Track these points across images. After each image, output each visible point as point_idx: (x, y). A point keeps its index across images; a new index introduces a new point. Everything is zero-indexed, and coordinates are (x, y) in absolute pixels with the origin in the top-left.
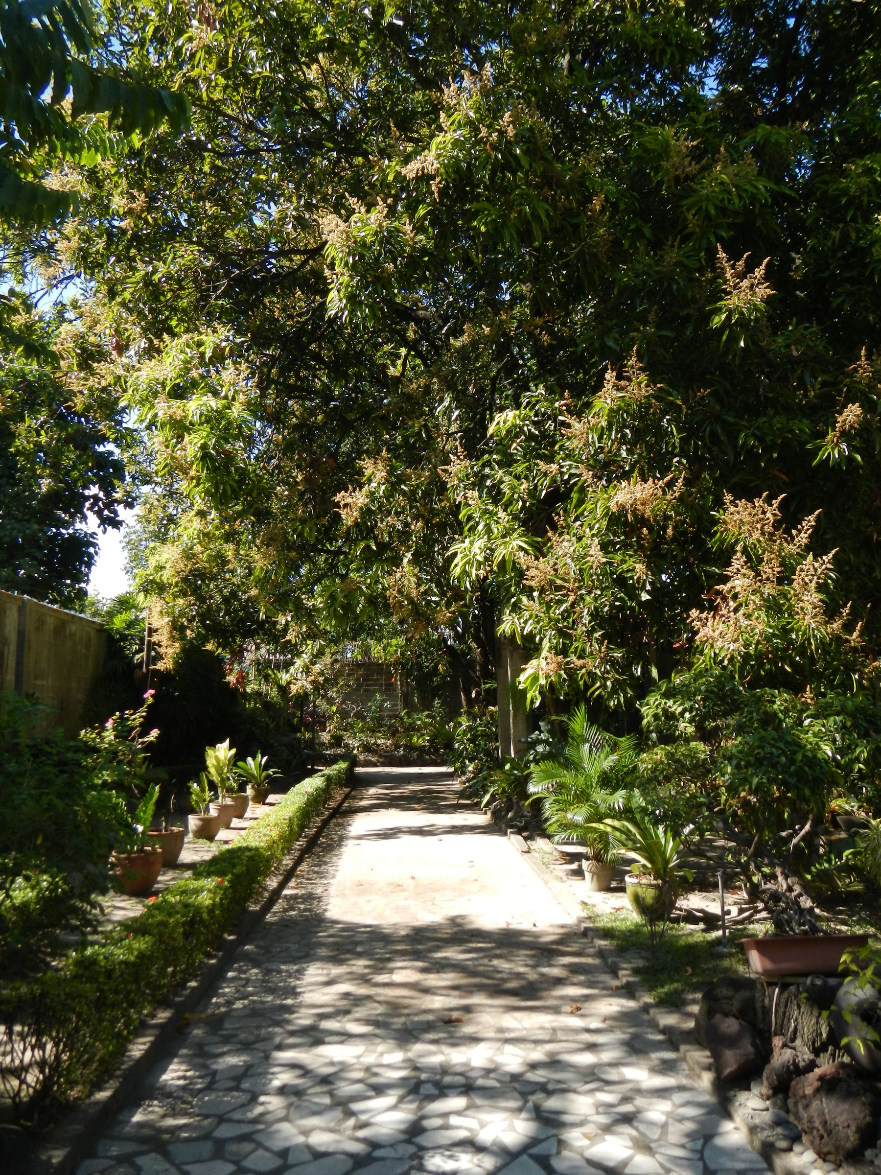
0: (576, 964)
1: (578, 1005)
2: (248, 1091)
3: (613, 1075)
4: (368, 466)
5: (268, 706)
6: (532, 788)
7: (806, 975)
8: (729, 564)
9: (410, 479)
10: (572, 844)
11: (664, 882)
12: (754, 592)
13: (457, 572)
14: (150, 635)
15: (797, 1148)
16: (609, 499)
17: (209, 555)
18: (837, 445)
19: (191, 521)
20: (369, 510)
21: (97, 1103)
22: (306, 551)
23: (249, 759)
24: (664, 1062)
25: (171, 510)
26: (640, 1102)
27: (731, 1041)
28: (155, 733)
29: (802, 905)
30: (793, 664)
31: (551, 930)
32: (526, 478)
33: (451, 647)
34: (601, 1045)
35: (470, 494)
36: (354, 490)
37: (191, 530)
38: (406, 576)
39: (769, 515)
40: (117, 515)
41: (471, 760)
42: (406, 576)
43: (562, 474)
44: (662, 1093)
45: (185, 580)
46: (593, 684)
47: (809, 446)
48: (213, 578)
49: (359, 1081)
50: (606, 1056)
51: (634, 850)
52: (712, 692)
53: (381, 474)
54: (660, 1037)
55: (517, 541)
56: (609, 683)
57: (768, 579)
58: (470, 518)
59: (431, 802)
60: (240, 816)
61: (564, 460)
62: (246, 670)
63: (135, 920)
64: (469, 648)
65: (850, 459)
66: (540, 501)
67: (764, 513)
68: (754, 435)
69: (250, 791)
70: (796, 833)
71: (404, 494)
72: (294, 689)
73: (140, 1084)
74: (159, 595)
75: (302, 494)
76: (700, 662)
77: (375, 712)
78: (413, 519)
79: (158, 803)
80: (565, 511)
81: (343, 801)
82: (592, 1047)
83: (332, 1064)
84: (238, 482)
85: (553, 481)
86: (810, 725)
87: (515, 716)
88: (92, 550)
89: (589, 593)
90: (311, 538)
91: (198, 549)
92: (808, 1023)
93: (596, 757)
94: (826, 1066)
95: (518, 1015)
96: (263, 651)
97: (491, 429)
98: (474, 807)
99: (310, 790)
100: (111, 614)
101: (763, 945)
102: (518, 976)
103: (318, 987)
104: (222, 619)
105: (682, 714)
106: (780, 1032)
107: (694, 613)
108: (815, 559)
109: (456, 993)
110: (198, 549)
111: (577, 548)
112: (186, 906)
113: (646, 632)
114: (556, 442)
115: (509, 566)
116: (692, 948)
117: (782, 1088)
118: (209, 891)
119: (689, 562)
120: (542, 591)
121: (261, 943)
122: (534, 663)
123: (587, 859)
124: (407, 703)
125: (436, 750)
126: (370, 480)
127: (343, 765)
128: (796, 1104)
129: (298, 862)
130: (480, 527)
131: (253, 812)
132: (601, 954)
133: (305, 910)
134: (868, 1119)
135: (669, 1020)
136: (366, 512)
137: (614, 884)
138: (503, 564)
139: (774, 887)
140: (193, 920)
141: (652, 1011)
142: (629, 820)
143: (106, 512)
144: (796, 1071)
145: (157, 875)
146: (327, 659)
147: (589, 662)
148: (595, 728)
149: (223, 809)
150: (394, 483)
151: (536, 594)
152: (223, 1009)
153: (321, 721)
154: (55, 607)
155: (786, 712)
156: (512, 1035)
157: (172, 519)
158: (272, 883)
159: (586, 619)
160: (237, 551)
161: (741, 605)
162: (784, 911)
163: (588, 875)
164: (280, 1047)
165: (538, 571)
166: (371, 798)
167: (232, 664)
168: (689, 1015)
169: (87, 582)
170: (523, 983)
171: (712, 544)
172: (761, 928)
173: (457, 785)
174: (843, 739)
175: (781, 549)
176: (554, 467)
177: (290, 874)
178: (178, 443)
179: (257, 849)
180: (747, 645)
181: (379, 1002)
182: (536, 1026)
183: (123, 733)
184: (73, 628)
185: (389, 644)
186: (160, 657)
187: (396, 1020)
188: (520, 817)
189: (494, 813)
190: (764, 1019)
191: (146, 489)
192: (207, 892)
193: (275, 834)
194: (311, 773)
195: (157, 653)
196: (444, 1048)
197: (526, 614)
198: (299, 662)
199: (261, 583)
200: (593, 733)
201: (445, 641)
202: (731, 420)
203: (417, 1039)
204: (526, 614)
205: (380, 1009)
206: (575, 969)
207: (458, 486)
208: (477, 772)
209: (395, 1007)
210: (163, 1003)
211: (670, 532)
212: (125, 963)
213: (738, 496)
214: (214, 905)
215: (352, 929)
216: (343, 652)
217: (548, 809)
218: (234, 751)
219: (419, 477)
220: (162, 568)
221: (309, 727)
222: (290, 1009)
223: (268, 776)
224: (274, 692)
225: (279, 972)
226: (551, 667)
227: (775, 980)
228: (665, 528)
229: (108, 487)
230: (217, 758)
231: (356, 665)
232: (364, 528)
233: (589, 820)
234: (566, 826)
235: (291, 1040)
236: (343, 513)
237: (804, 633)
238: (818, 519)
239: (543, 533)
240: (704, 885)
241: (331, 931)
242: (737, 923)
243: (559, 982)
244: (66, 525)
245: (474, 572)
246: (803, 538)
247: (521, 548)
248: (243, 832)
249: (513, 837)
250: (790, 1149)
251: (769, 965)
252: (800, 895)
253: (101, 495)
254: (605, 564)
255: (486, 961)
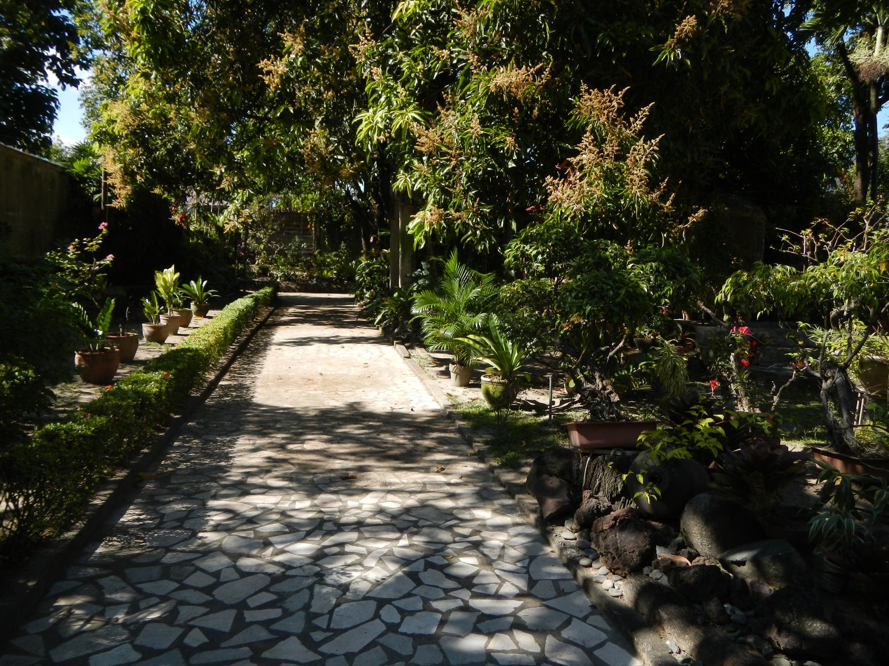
0: (442, 438)
1: (442, 467)
2: (189, 529)
3: (466, 515)
4: (288, 40)
5: (208, 242)
6: (414, 311)
7: (611, 449)
8: (580, 141)
9: (324, 54)
10: (443, 352)
11: (510, 382)
12: (597, 165)
13: (361, 136)
14: (106, 179)
15: (595, 565)
16: (489, 81)
17: (154, 113)
18: (673, 50)
19: (137, 82)
20: (288, 78)
21: (66, 540)
22: (237, 115)
23: (192, 282)
24: (504, 506)
25: (120, 71)
26: (485, 534)
27: (553, 493)
28: (110, 258)
29: (612, 399)
30: (619, 223)
31: (424, 413)
32: (422, 60)
33: (355, 202)
34: (459, 495)
35: (375, 70)
36: (276, 59)
37: (137, 90)
38: (318, 137)
39: (614, 103)
40: (74, 74)
41: (368, 290)
42: (318, 137)
43: (452, 59)
44: (502, 528)
45: (133, 133)
46: (467, 232)
47: (651, 49)
48: (158, 132)
49: (277, 521)
50: (461, 503)
51: (489, 357)
52: (560, 240)
53: (299, 47)
54: (501, 489)
55: (412, 113)
56: (478, 232)
57: (608, 155)
58: (374, 91)
59: (337, 320)
60: (186, 326)
61: (454, 47)
62: (189, 208)
63: (94, 402)
64: (370, 204)
65: (682, 63)
66: (432, 81)
67: (611, 101)
68: (609, 37)
69: (193, 307)
70: (612, 348)
71: (317, 65)
72: (227, 228)
73: (103, 524)
74: (113, 145)
75: (232, 63)
76: (550, 219)
77: (294, 250)
78: (325, 89)
79: (114, 313)
80: (452, 90)
81: (268, 317)
82: (452, 496)
83: (256, 508)
84: (175, 46)
85: (444, 65)
86: (632, 268)
87: (403, 257)
88: (53, 104)
89: (468, 159)
90: (239, 99)
91: (144, 107)
92: (609, 481)
93: (464, 286)
94: (619, 510)
95: (398, 473)
96: (202, 196)
97: (395, 16)
98: (369, 324)
99: (241, 307)
100: (72, 160)
101: (581, 427)
102: (400, 445)
103: (247, 453)
104: (167, 170)
105: (536, 256)
106: (588, 487)
107: (549, 179)
108: (645, 142)
109: (352, 458)
110: (144, 107)
111: (460, 122)
112: (136, 392)
113: (511, 193)
114: (448, 31)
115: (405, 134)
116: (526, 428)
117: (587, 525)
118: (156, 381)
119: (547, 137)
120: (430, 156)
121: (202, 420)
122: (421, 213)
123: (453, 363)
124: (320, 244)
125: (342, 282)
126: (290, 53)
127: (268, 290)
128: (597, 537)
129: (232, 361)
130: (382, 99)
131: (196, 323)
132: (460, 430)
133: (237, 396)
134: (648, 547)
135: (509, 477)
136: (286, 80)
137: (472, 382)
138: (399, 131)
139: (593, 387)
140: (143, 401)
141: (496, 471)
142: (486, 336)
143: (64, 72)
144: (598, 513)
145: (117, 368)
146: (255, 206)
147: (463, 214)
148: (464, 266)
149: (170, 320)
150: (310, 56)
151: (425, 158)
152: (170, 469)
153: (252, 256)
154: (21, 150)
155: (615, 258)
156: (393, 488)
157: (121, 81)
158: (211, 376)
159: (464, 180)
160: (178, 110)
161: (585, 175)
162: (599, 403)
163: (453, 375)
164: (215, 497)
165: (428, 138)
166: (290, 315)
167: (177, 206)
168: (524, 473)
169: (52, 131)
170: (403, 451)
171: (568, 125)
172: (579, 415)
173: (357, 307)
174: (656, 280)
175: (620, 133)
176: (446, 52)
177: (225, 370)
178: (120, 6)
179: (197, 350)
180: (587, 207)
181: (292, 464)
182: (411, 481)
183: (85, 257)
184: (39, 169)
185: (306, 198)
186: (115, 197)
187: (306, 477)
188: (404, 332)
189: (384, 329)
190: (578, 478)
191: (98, 53)
192: (154, 383)
193: (212, 339)
194: (242, 295)
195: (113, 194)
196: (342, 497)
197: (417, 174)
198: (231, 207)
199: (199, 137)
200: (464, 272)
201: (351, 197)
202: (592, 21)
203: (321, 491)
204: (417, 174)
205: (293, 469)
206: (442, 441)
207: (365, 63)
208: (372, 298)
209: (305, 468)
210: (122, 466)
211: (536, 112)
212: (84, 436)
213: (591, 86)
214: (160, 392)
215: (273, 410)
216: (270, 201)
217: (426, 326)
218: (178, 274)
219: (331, 52)
220: (114, 122)
221: (242, 260)
222: (223, 470)
223: (208, 296)
224: (213, 231)
225: (216, 442)
226: (434, 217)
227: (588, 452)
228: (532, 109)
229: (63, 49)
230: (164, 280)
231: (279, 214)
232: (286, 95)
233: (456, 335)
234: (438, 339)
235: (224, 492)
236: (267, 80)
237: (631, 200)
238: (651, 111)
239: (433, 108)
240: (538, 383)
241: (256, 412)
242: (558, 410)
243: (430, 450)
244: (24, 79)
245: (376, 137)
246: (638, 125)
247: (415, 119)
248: (185, 338)
249: (398, 346)
250: (590, 566)
251: (585, 441)
252: (611, 392)
253: (58, 55)
254: (482, 135)
255: (375, 435)
